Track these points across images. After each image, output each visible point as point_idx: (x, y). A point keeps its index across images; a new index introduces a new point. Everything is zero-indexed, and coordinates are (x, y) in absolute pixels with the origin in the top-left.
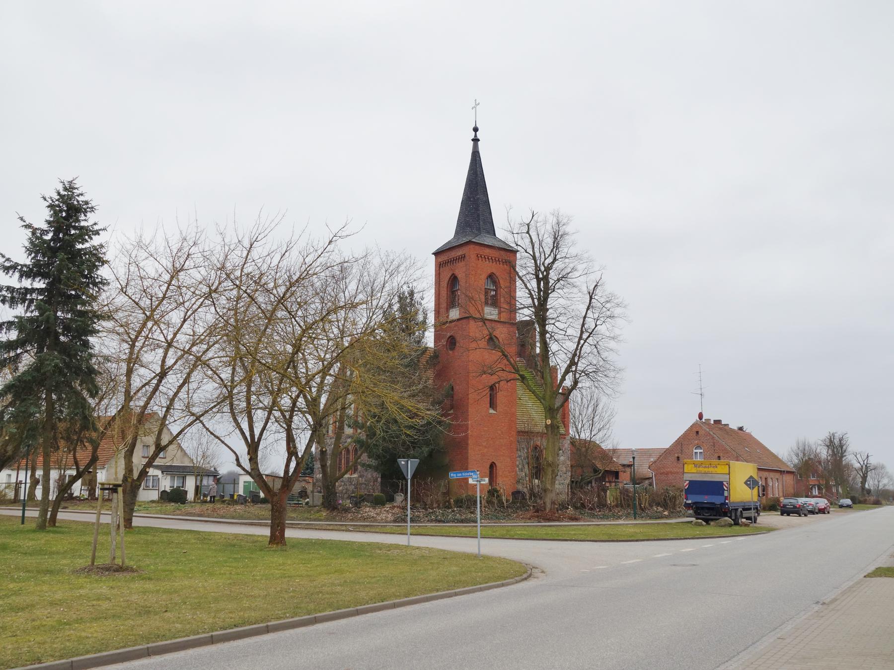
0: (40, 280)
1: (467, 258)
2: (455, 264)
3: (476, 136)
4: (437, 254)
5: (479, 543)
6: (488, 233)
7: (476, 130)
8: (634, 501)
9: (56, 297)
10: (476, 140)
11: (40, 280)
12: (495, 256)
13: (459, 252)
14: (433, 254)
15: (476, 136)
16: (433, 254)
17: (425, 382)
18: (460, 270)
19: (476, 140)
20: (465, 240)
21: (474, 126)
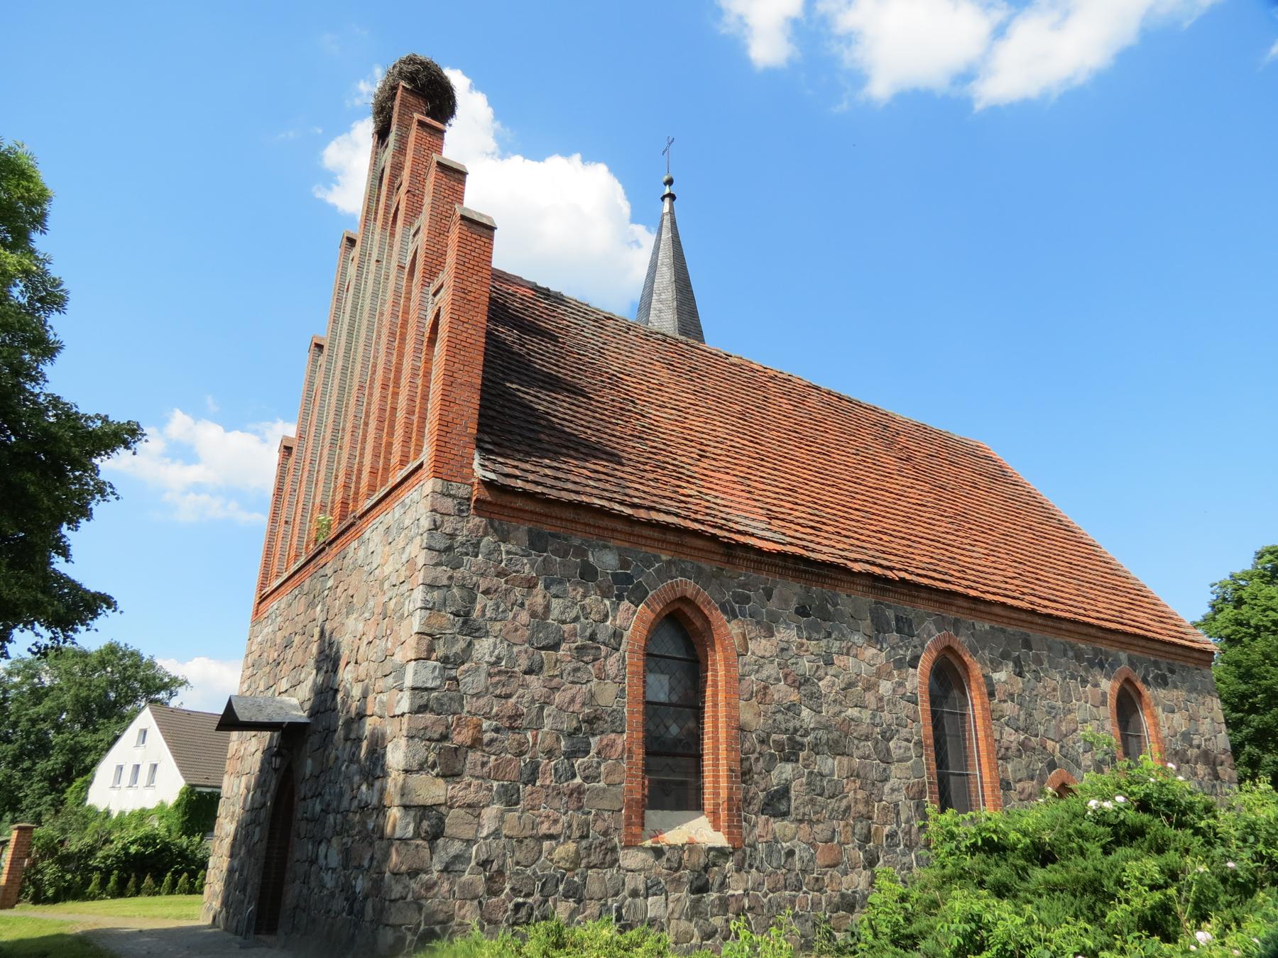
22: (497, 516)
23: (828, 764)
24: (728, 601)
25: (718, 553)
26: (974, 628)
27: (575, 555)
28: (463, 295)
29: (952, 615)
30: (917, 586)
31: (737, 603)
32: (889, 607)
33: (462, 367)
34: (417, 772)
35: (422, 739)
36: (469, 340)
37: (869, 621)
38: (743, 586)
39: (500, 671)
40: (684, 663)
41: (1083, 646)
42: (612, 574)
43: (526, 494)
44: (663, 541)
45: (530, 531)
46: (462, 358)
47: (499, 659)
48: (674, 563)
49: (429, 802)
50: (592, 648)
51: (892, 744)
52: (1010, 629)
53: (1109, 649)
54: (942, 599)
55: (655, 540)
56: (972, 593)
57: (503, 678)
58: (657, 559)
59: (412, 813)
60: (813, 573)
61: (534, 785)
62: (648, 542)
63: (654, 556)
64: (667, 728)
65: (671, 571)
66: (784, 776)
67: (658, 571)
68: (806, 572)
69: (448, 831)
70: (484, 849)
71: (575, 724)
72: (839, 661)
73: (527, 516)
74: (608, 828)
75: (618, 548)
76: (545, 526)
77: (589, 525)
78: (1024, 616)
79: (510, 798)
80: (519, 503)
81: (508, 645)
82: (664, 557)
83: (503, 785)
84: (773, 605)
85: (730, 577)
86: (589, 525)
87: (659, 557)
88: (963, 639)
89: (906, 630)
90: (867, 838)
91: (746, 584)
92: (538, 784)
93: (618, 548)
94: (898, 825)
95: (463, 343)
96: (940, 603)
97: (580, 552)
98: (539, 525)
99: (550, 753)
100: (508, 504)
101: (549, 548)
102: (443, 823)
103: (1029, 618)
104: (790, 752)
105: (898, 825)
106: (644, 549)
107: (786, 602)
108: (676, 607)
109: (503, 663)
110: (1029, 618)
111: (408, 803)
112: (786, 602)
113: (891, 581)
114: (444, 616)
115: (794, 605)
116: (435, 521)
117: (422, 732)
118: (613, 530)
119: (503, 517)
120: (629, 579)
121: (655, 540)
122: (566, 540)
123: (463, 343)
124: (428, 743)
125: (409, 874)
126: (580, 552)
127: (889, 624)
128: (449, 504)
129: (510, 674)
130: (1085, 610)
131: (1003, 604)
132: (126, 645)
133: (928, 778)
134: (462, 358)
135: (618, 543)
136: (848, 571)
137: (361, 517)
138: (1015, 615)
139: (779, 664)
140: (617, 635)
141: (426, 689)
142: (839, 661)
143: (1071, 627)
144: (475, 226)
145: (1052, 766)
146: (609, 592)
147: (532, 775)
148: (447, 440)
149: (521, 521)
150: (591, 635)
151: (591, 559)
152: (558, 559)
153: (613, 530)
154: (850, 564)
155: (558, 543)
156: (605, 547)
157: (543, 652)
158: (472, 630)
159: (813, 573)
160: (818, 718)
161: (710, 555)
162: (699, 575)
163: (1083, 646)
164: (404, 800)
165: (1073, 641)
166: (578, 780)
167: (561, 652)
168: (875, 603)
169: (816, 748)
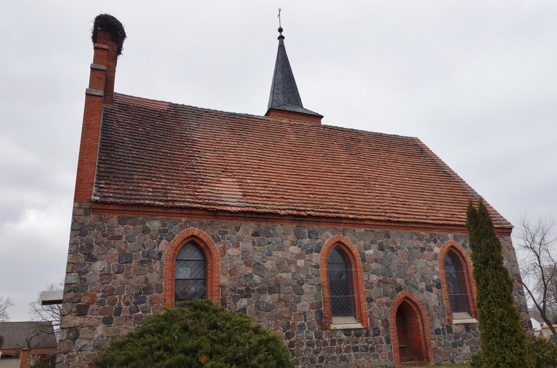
7: (280, 30)
10: (281, 38)
19: (281, 38)
22: (103, 213)
23: (268, 298)
24: (216, 235)
25: (210, 215)
26: (355, 232)
27: (140, 224)
28: (87, 127)
29: (341, 228)
30: (319, 217)
31: (221, 234)
32: (305, 228)
33: (87, 156)
34: (67, 315)
35: (70, 302)
36: (90, 145)
37: (293, 235)
38: (224, 227)
39: (106, 275)
40: (202, 262)
41: (424, 233)
42: (157, 230)
43: (112, 203)
44: (182, 214)
45: (118, 217)
46: (87, 152)
47: (104, 269)
48: (189, 222)
49: (72, 326)
50: (148, 260)
51: (303, 287)
52: (377, 230)
53: (440, 233)
54: (334, 221)
55: (178, 214)
56: (351, 216)
57: (106, 277)
58: (180, 221)
59: (65, 331)
60: (261, 218)
61: (120, 316)
62: (175, 215)
63: (178, 220)
64: (190, 289)
65: (187, 225)
66: (243, 304)
67: (180, 226)
68: (257, 218)
69: (81, 336)
70: (97, 342)
71: (139, 291)
72: (274, 253)
73: (117, 212)
74: (199, 347)
75: (160, 219)
76: (125, 215)
77: (145, 212)
78: (384, 224)
79: (108, 321)
80: (112, 207)
81: (108, 263)
82: (183, 220)
83: (105, 317)
84: (239, 234)
85: (217, 224)
86: (145, 212)
87: (181, 220)
88: (348, 237)
89: (314, 237)
90: (288, 326)
91: (225, 226)
92: (121, 315)
93: (160, 219)
94: (305, 321)
95: (87, 146)
96: (334, 223)
97: (143, 223)
98: (123, 215)
99: (127, 304)
100: (107, 208)
101: (128, 223)
102: (78, 333)
103: (388, 224)
104: (247, 293)
105: (305, 321)
106: (173, 218)
107: (247, 231)
108: (191, 239)
109: (106, 271)
110: (388, 224)
111: (63, 327)
112: (247, 231)
113: (303, 216)
114: (79, 255)
115: (251, 232)
116: (75, 219)
117: (69, 300)
118: (158, 212)
119: (101, 213)
120: (166, 231)
121: (178, 214)
122: (135, 218)
123: (87, 146)
124: (72, 304)
125: (64, 353)
126: (143, 223)
127: (304, 235)
128: (81, 211)
129: (110, 275)
130: (427, 216)
131: (370, 219)
132: (30, 313)
133: (323, 300)
134: (87, 152)
135: (160, 217)
136: (278, 215)
137: (540, 263)
138: (379, 224)
139: (242, 258)
140: (160, 254)
141: (71, 284)
142: (274, 253)
143: (415, 225)
144: (92, 97)
145: (399, 289)
146: (156, 237)
147: (118, 312)
148: (80, 186)
149: (114, 214)
150: (147, 255)
151: (147, 225)
152: (132, 227)
153: (158, 212)
154: (279, 212)
155: (132, 221)
156: (154, 219)
157: (124, 264)
158: (92, 259)
159: (261, 218)
160: (262, 279)
161: (206, 217)
162: (201, 225)
163: (424, 233)
164: (62, 326)
165: (416, 231)
166: (140, 313)
167: (133, 264)
168: (297, 226)
169: (261, 291)
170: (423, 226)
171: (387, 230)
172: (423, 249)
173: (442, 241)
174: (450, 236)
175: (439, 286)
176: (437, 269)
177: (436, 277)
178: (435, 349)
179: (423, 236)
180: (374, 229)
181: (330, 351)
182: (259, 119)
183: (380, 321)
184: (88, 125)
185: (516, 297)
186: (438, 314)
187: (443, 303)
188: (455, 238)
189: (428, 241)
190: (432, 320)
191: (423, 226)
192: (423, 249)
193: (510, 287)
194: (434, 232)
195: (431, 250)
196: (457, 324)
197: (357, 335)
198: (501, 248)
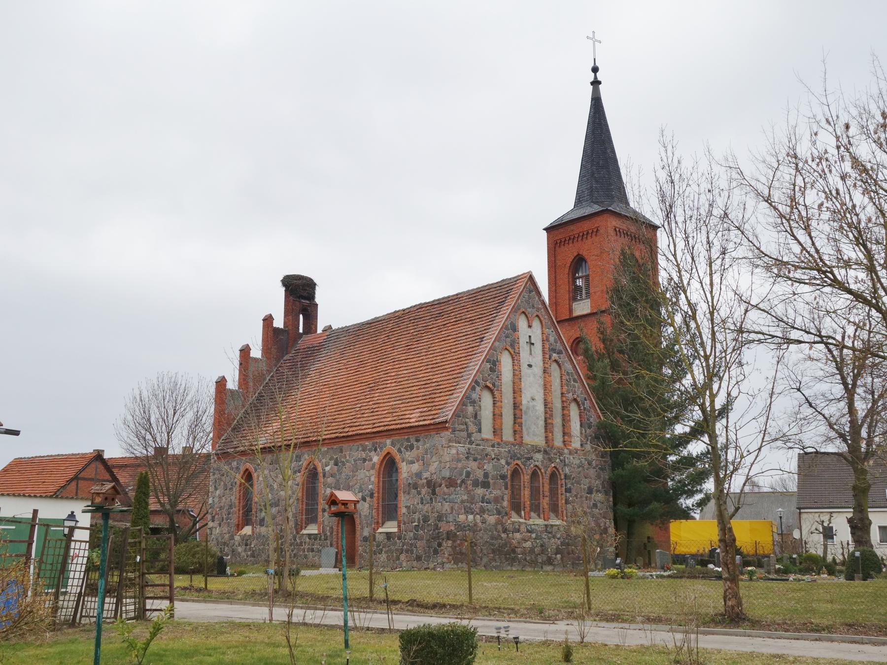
0: (704, 551)
1: (602, 231)
2: (584, 240)
3: (596, 77)
4: (547, 229)
5: (24, 542)
6: (621, 202)
7: (595, 70)
8: (456, 441)
9: (501, 347)
10: (596, 83)
11: (704, 551)
12: (621, 227)
13: (587, 226)
14: (544, 229)
15: (596, 77)
16: (544, 229)
17: (626, 379)
18: (587, 248)
19: (596, 83)
20: (596, 208)
21: (592, 65)
52: (335, 447)
143: (358, 437)
170: (365, 437)
171: (340, 445)
172: (365, 460)
173: (381, 449)
174: (388, 442)
175: (372, 496)
176: (373, 479)
177: (370, 487)
178: (361, 555)
179: (366, 446)
180: (332, 446)
181: (299, 550)
182: (367, 324)
183: (328, 528)
184: (620, 188)
185: (440, 504)
186: (367, 523)
187: (372, 513)
188: (393, 444)
189: (370, 451)
190: (362, 529)
191: (365, 437)
192: (365, 460)
193: (340, 505)
194: (375, 441)
195: (371, 460)
196: (381, 533)
197: (315, 539)
198: (108, 519)
